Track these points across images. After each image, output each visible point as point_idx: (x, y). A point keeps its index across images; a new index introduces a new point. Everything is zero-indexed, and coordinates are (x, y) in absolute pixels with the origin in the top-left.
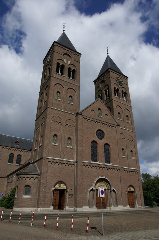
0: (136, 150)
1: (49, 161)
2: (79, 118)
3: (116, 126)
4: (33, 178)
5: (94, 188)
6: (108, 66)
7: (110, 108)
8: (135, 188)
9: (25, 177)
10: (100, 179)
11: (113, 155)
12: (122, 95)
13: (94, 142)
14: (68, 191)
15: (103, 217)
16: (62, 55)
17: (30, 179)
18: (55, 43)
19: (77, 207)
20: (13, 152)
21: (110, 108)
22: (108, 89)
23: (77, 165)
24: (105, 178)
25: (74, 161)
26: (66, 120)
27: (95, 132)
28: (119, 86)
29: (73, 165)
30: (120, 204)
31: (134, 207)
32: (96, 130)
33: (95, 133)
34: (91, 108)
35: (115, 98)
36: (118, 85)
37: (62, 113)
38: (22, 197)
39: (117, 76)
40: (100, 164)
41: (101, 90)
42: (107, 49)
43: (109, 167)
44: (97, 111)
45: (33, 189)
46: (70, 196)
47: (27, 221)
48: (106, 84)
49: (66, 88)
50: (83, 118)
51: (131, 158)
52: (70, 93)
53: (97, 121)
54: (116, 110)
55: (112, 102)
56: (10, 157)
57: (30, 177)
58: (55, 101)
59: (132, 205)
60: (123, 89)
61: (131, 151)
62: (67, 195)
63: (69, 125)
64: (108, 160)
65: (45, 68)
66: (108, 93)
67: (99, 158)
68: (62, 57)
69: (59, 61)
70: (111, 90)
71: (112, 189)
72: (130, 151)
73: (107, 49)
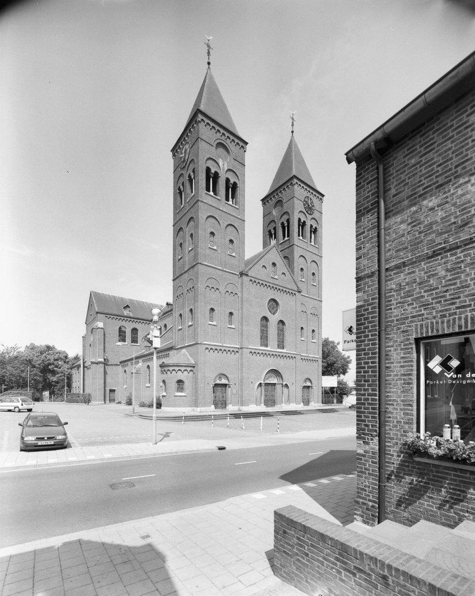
0: (319, 329)
1: (207, 348)
2: (244, 282)
3: (296, 293)
5: (262, 382)
6: (291, 169)
7: (288, 259)
8: (312, 381)
10: (272, 369)
11: (289, 338)
12: (309, 231)
13: (265, 319)
14: (231, 386)
16: (214, 148)
18: (200, 115)
19: (242, 406)
20: (124, 323)
21: (288, 259)
22: (194, 171)
23: (242, 352)
26: (225, 284)
27: (267, 302)
29: (237, 352)
30: (293, 402)
31: (308, 404)
32: (268, 300)
33: (267, 304)
34: (261, 263)
35: (297, 239)
37: (220, 273)
39: (305, 194)
41: (273, 221)
43: (282, 354)
44: (270, 268)
45: (187, 385)
48: (285, 211)
49: (224, 225)
50: (251, 280)
51: (312, 341)
52: (231, 233)
53: (260, 281)
54: (298, 263)
55: (293, 249)
58: (208, 251)
59: (307, 402)
61: (313, 331)
63: (230, 292)
64: (281, 345)
65: (180, 172)
66: (286, 228)
67: (271, 343)
68: (213, 152)
69: (210, 164)
70: (293, 225)
71: (284, 383)
72: (311, 331)
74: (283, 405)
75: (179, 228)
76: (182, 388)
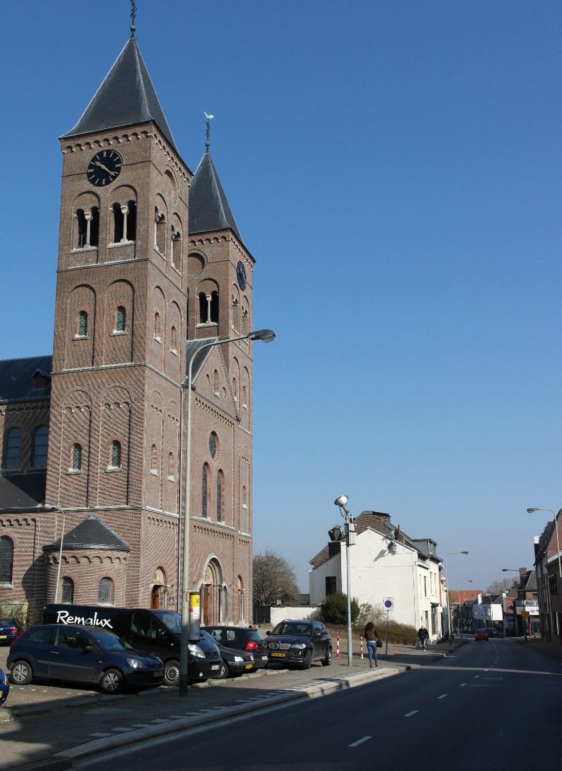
25: (177, 516)
37: (164, 382)
40: (213, 525)
46: (170, 600)
71: (224, 585)
76: (107, 595)
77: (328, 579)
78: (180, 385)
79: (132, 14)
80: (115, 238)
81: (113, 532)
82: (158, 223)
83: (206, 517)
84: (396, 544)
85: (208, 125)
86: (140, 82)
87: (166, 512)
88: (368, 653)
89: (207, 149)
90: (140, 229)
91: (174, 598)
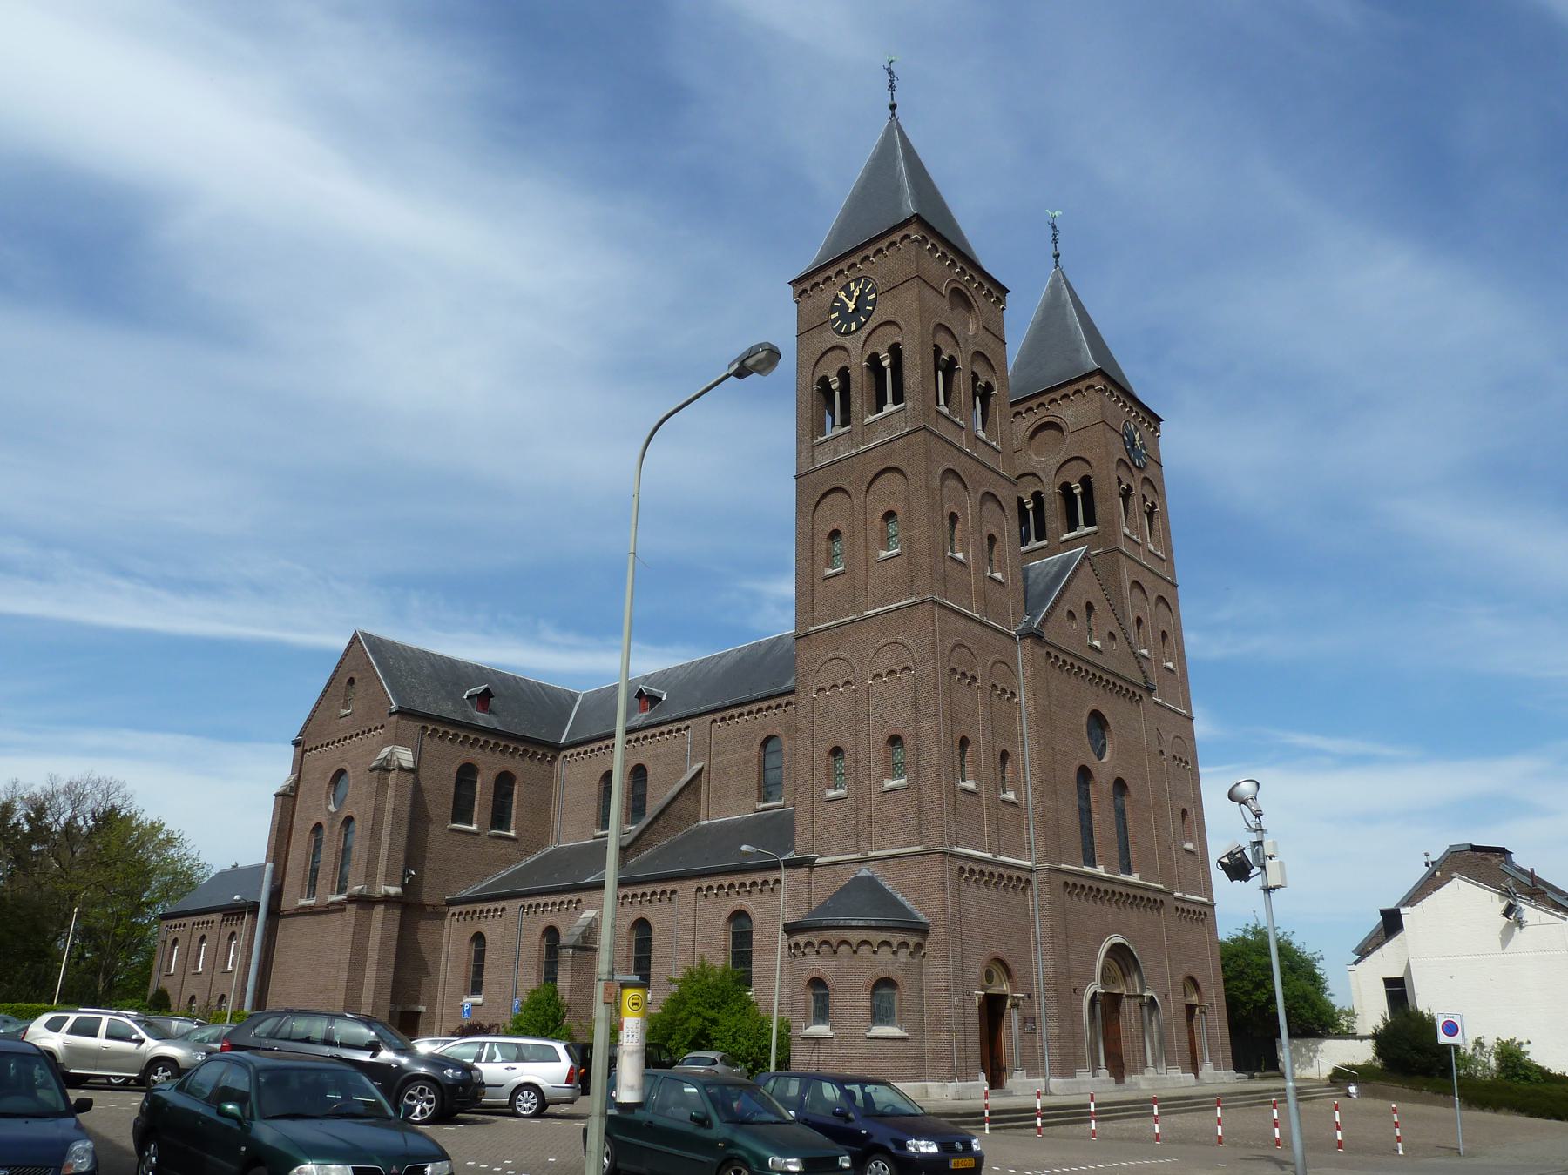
4: (871, 945)
9: (851, 940)
15: (1458, 1112)
17: (875, 952)
20: (474, 755)
24: (1127, 944)
28: (1134, 469)
36: (1130, 464)
38: (869, 1034)
40: (1110, 881)
42: (890, 73)
47: (1130, 1126)
56: (459, 782)
57: (855, 942)
60: (1147, 490)
62: (1012, 1021)
71: (1148, 994)
73: (890, 73)
74: (1150, 1073)
75: (826, 488)
77: (1389, 982)
78: (1014, 633)
79: (1054, 240)
80: (877, 408)
81: (899, 896)
82: (1148, 514)
83: (1130, 874)
84: (1523, 906)
85: (1054, 227)
86: (901, 171)
87: (1188, 896)
88: (278, 1037)
89: (1057, 262)
90: (1100, 510)
91: (1034, 1019)
